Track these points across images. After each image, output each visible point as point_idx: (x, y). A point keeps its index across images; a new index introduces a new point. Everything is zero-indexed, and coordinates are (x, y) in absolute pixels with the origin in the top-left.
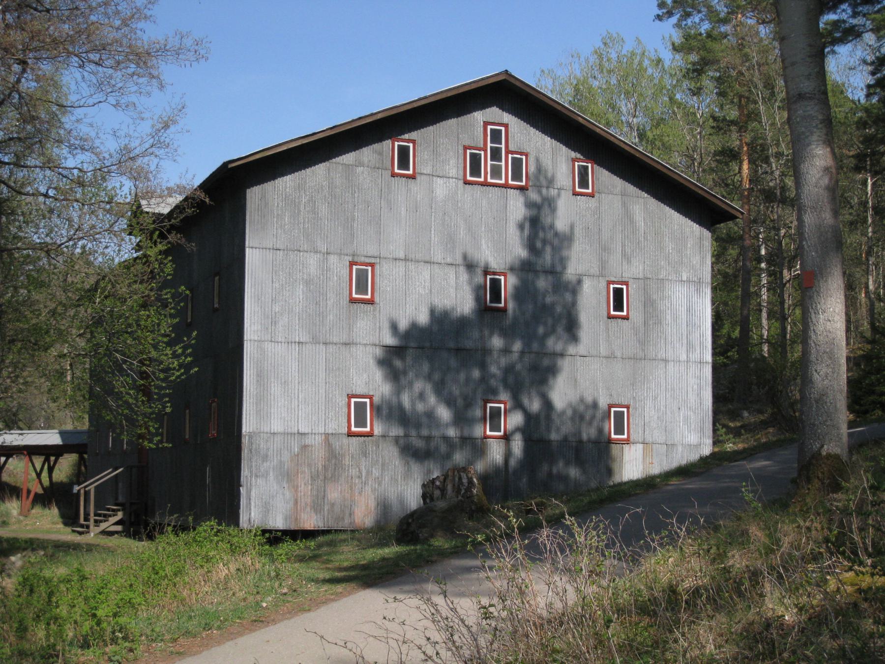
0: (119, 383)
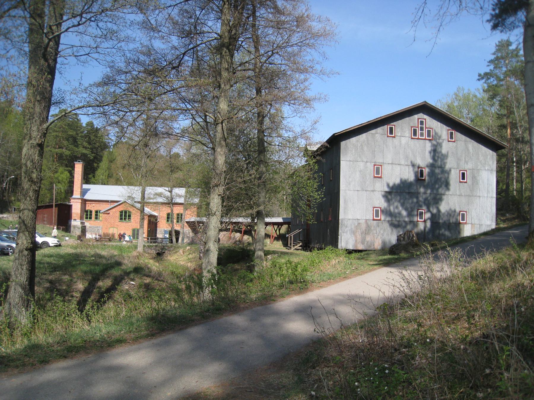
0: (301, 203)
